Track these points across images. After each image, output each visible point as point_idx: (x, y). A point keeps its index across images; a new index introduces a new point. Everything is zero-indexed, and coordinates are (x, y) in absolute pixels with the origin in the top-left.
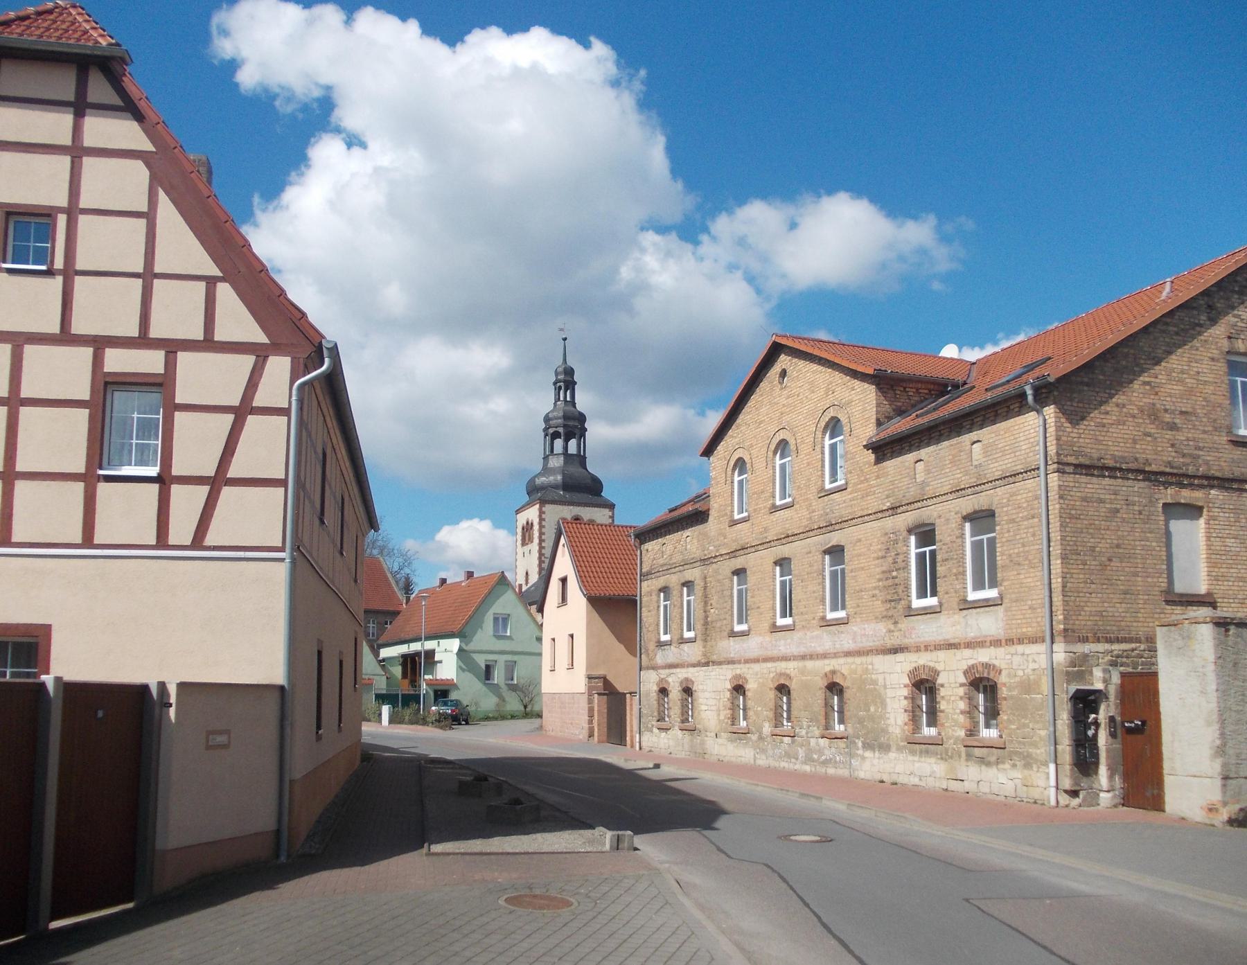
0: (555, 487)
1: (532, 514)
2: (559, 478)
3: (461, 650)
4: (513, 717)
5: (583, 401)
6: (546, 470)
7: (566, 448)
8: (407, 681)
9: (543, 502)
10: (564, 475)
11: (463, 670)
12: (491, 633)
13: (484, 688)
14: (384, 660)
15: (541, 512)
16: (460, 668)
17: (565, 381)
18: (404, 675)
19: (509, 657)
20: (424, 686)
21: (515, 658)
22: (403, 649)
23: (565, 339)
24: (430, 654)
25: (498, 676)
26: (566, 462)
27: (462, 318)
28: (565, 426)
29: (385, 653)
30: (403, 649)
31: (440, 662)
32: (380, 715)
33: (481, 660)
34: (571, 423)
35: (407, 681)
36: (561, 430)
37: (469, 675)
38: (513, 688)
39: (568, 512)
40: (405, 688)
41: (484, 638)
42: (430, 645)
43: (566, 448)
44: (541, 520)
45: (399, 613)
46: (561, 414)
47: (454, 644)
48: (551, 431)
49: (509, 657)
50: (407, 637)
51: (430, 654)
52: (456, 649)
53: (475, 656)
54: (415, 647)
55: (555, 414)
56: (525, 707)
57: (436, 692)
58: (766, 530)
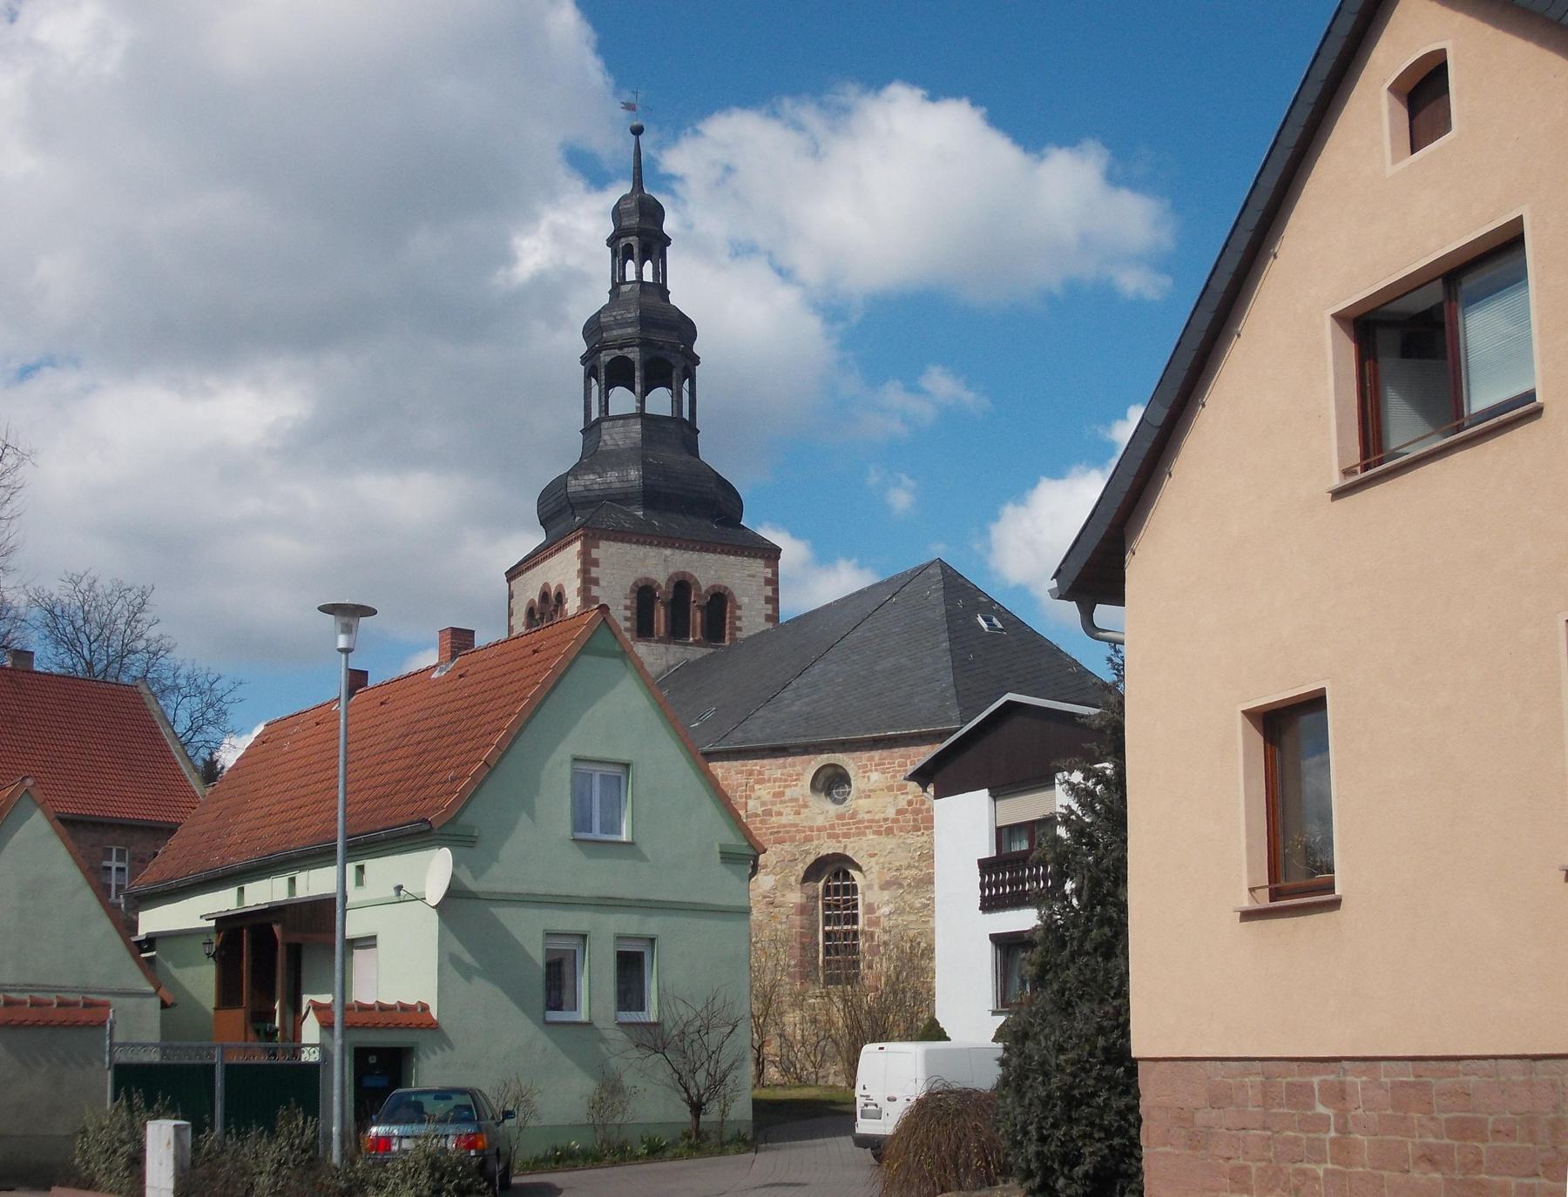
0: (622, 498)
1: (563, 571)
2: (634, 474)
3: (455, 901)
4: (655, 1151)
5: (690, 285)
6: (593, 456)
7: (640, 274)
8: (237, 1017)
9: (593, 535)
10: (646, 466)
11: (467, 973)
12: (565, 829)
13: (542, 1040)
14: (151, 941)
15: (588, 563)
16: (449, 962)
17: (640, 233)
18: (228, 994)
19: (630, 923)
20: (311, 1030)
21: (652, 925)
22: (223, 901)
23: (637, 131)
24: (323, 912)
25: (593, 989)
26: (647, 437)
27: (191, 330)
28: (645, 344)
29: (152, 921)
30: (223, 901)
31: (369, 942)
32: (137, 1161)
33: (530, 932)
34: (659, 337)
35: (238, 1016)
36: (634, 354)
37: (484, 990)
38: (652, 1039)
39: (659, 564)
40: (229, 1044)
41: (537, 846)
42: (315, 882)
43: (640, 274)
44: (588, 581)
45: (169, 830)
46: (633, 314)
47: (433, 870)
48: (605, 357)
49: (630, 923)
50: (237, 862)
51: (323, 912)
52: (435, 891)
53: (508, 917)
54: (265, 892)
55: (617, 313)
56: (697, 1108)
57: (361, 1055)
58: (859, 868)
